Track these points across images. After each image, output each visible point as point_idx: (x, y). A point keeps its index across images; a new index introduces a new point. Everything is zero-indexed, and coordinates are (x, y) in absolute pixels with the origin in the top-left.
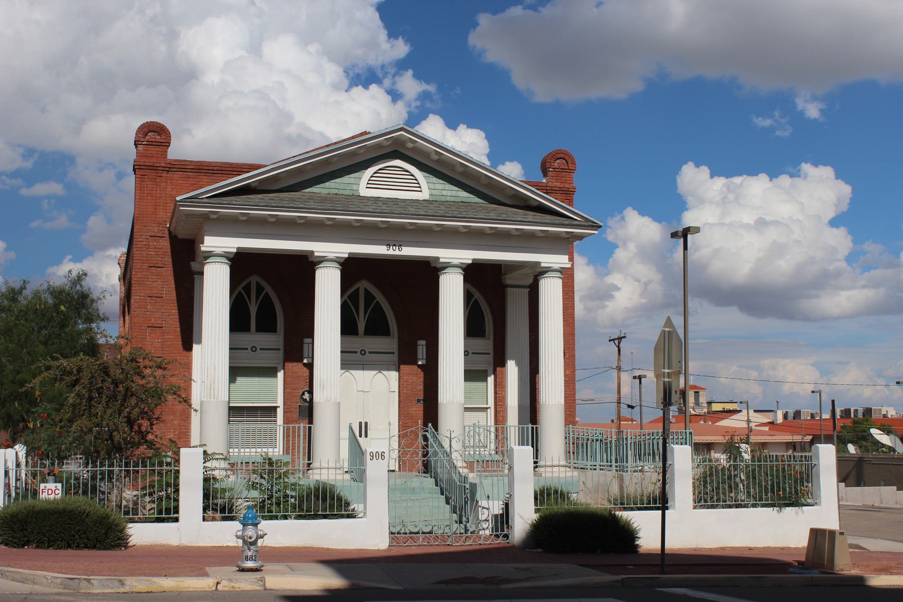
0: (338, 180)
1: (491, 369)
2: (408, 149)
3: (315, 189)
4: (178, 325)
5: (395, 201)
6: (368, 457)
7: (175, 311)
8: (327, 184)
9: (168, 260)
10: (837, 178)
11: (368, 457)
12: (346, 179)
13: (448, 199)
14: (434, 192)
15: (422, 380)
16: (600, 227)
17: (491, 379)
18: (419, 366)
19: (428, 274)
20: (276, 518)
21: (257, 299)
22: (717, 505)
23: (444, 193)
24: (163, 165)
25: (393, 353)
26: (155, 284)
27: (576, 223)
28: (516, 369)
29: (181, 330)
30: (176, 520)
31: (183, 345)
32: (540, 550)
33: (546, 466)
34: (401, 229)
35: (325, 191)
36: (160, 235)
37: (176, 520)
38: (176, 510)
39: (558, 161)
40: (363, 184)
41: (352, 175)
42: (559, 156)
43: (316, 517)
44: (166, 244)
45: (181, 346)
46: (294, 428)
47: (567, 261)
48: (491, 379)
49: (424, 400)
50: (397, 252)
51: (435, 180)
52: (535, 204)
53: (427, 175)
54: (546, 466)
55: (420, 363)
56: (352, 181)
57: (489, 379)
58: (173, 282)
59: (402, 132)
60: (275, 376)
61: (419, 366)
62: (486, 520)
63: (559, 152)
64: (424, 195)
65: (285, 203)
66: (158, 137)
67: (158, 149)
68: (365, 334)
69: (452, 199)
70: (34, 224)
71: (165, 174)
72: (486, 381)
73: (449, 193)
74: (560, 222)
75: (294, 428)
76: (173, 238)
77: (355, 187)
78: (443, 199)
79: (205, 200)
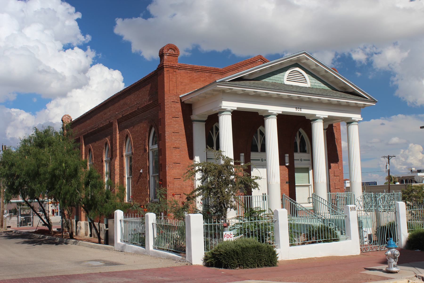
0: (275, 76)
2: (301, 63)
6: (350, 210)
7: (185, 140)
8: (271, 78)
9: (180, 114)
10: (109, 69)
12: (278, 76)
13: (318, 87)
14: (313, 84)
15: (287, 173)
18: (286, 166)
22: (107, 232)
23: (316, 84)
24: (177, 66)
25: (309, 160)
26: (176, 126)
29: (188, 150)
30: (291, 245)
32: (418, 250)
35: (271, 81)
36: (176, 101)
40: (285, 78)
41: (281, 74)
44: (179, 106)
46: (247, 197)
47: (360, 117)
48: (311, 172)
49: (289, 182)
50: (300, 112)
51: (312, 78)
52: (351, 91)
55: (287, 165)
56: (281, 77)
57: (310, 171)
58: (183, 125)
60: (308, 172)
61: (286, 166)
62: (366, 237)
64: (308, 85)
66: (174, 52)
67: (173, 58)
71: (177, 71)
73: (317, 84)
76: (183, 104)
77: (282, 80)
78: (315, 87)
79: (229, 83)
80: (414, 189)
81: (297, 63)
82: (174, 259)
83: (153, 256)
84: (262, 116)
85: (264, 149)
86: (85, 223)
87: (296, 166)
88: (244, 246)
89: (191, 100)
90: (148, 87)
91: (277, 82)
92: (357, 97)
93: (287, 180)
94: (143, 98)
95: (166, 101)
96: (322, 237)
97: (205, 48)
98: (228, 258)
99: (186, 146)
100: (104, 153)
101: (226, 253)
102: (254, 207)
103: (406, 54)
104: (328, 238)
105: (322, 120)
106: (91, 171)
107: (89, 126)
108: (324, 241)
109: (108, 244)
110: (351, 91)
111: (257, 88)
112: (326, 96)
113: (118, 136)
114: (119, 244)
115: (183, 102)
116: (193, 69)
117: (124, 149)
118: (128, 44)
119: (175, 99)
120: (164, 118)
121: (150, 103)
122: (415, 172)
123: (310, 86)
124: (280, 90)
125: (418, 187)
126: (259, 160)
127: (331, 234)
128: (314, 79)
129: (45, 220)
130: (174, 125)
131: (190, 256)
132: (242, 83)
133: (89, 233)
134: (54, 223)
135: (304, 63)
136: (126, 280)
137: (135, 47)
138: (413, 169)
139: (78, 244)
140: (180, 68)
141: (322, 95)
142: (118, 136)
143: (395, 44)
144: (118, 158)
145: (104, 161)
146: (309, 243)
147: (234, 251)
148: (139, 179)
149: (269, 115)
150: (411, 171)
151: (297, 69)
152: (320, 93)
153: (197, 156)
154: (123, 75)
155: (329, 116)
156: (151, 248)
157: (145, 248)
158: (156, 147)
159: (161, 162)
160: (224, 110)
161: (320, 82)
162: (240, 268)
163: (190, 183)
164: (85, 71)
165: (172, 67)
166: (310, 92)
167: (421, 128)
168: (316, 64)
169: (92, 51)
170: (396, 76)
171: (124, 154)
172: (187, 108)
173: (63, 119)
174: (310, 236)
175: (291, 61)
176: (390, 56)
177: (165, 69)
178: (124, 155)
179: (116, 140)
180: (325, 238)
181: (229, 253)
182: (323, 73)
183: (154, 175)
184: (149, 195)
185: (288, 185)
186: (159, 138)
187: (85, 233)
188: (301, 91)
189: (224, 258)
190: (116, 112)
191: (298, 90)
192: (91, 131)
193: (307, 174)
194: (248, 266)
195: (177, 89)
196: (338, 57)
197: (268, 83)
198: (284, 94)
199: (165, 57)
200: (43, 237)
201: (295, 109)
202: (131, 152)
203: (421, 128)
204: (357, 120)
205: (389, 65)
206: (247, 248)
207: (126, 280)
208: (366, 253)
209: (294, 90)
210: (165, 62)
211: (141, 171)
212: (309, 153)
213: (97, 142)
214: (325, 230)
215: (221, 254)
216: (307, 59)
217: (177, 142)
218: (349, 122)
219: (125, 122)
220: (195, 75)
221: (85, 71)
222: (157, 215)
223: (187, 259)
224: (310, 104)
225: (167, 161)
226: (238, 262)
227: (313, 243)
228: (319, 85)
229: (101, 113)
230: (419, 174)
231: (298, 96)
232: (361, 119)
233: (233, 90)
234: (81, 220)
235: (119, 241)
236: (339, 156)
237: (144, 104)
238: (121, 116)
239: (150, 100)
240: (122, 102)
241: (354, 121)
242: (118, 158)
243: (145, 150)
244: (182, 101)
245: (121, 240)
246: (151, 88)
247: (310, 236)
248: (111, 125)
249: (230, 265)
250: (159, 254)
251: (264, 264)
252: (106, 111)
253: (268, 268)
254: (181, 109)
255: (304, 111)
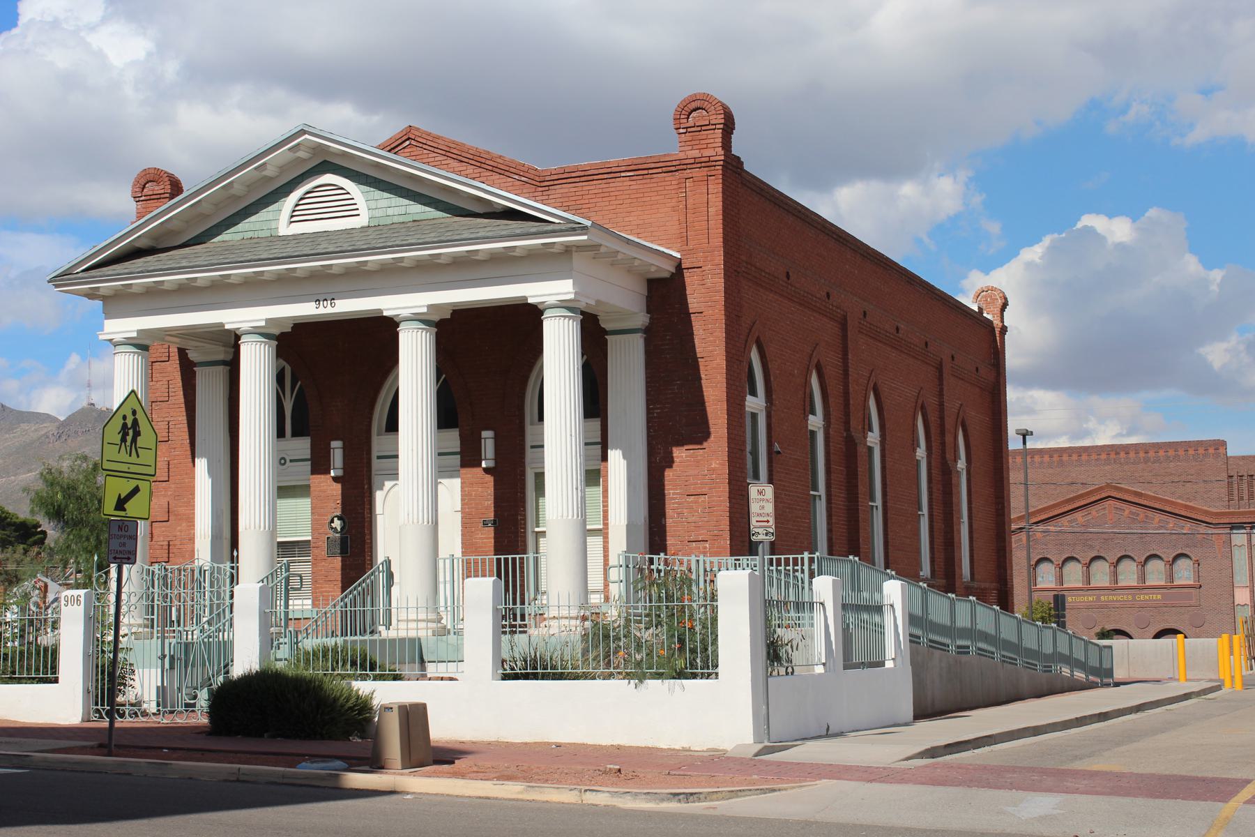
0: (253, 218)
3: (226, 236)
8: (240, 227)
13: (396, 220)
15: (491, 491)
19: (379, 336)
23: (390, 211)
27: (550, 227)
28: (208, 482)
30: (56, 681)
33: (428, 621)
35: (239, 237)
37: (56, 681)
38: (54, 669)
39: (694, 114)
40: (281, 220)
41: (270, 208)
42: (694, 105)
43: (19, 681)
46: (506, 560)
50: (329, 310)
51: (378, 194)
54: (428, 621)
59: (307, 136)
63: (694, 99)
65: (200, 261)
69: (401, 219)
70: (1088, 220)
73: (397, 211)
74: (534, 230)
75: (506, 560)
81: (325, 161)
93: (491, 516)
102: (153, 671)
128: (386, 195)
132: (139, 263)
134: (264, 654)
151: (328, 178)
161: (406, 202)
185: (490, 532)
197: (229, 247)
224: (359, 280)
228: (402, 210)
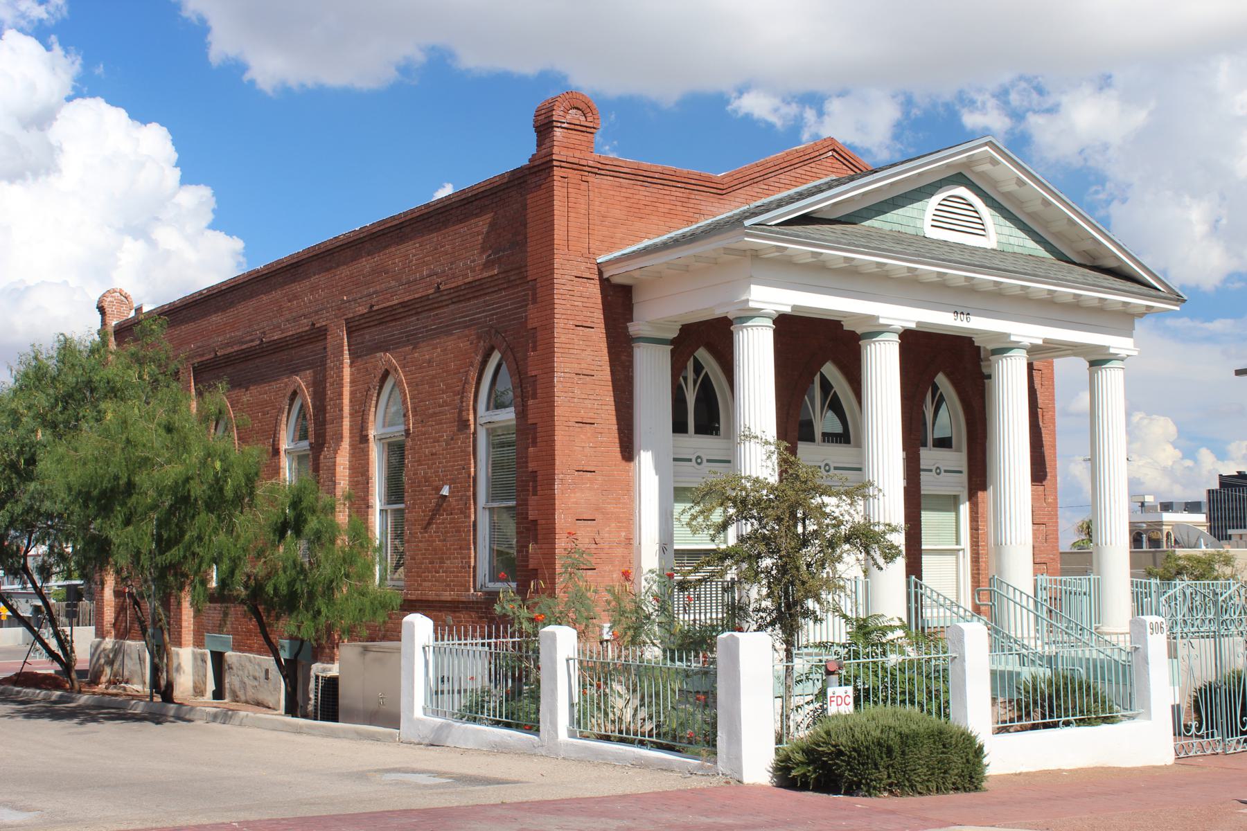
0: (900, 211)
1: (964, 494)
4: (615, 421)
5: (962, 247)
6: (1149, 630)
7: (610, 399)
8: (889, 216)
9: (599, 315)
11: (1149, 630)
13: (1017, 250)
16: (1184, 301)
17: (965, 509)
20: (1055, 725)
21: (695, 382)
23: (1012, 240)
24: (591, 163)
25: (960, 472)
31: (622, 452)
34: (970, 289)
35: (887, 227)
40: (924, 218)
41: (915, 205)
44: (594, 290)
45: (619, 455)
47: (1131, 346)
50: (965, 324)
51: (1001, 220)
53: (994, 213)
58: (605, 351)
59: (987, 148)
60: (956, 510)
64: (989, 242)
66: (583, 118)
68: (696, 432)
71: (591, 178)
72: (957, 511)
76: (605, 284)
79: (777, 229)
80: (1184, 567)
82: (666, 768)
83: (564, 757)
84: (853, 332)
85: (845, 436)
86: (194, 654)
87: (925, 490)
88: (907, 731)
89: (637, 274)
90: (482, 224)
91: (903, 229)
92: (1129, 284)
94: (464, 255)
95: (557, 274)
96: (1066, 710)
97: (472, 60)
98: (863, 764)
99: (614, 418)
100: (283, 426)
101: (854, 750)
103: (1140, 117)
104: (1089, 711)
105: (1024, 353)
106: (300, 489)
107: (222, 333)
108: (1081, 722)
109: (336, 720)
110: (1111, 264)
111: (853, 246)
112: (1045, 278)
113: (347, 372)
114: (419, 720)
115: (607, 279)
116: (640, 176)
117: (371, 418)
118: (200, 31)
119: (583, 268)
120: (549, 327)
121: (485, 275)
122: (1153, 508)
123: (994, 246)
124: (919, 256)
125: (1199, 560)
126: (690, 460)
127: (1088, 695)
128: (1008, 223)
129: (53, 644)
130: (579, 350)
131: (736, 759)
133: (211, 686)
135: (983, 175)
136: (615, 823)
137: (223, 43)
138: (1149, 499)
139: (236, 721)
140: (600, 169)
141: (1033, 276)
142: (347, 372)
143: (1104, 83)
144: (346, 444)
145: (282, 453)
146: (1024, 729)
147: (879, 744)
148: (431, 519)
149: (875, 333)
150: (1143, 504)
151: (962, 191)
152: (1029, 270)
153: (647, 449)
154: (175, 142)
155: (1046, 341)
156: (563, 734)
157: (538, 735)
158: (507, 416)
159: (532, 466)
160: (755, 314)
161: (1023, 235)
162: (891, 792)
163: (623, 534)
164: (41, 120)
165: (577, 167)
166: (1002, 265)
167: (1238, 373)
168: (1019, 179)
169: (67, 52)
170: (1108, 185)
171: (372, 433)
172: (618, 300)
173: (106, 305)
174: (1027, 706)
175: (948, 165)
176: (1086, 121)
177: (557, 172)
178: (371, 437)
179: (341, 386)
180: (1081, 712)
181: (867, 748)
182: (1037, 207)
183: (495, 505)
184: (475, 567)
186: (531, 390)
187: (195, 688)
188: (976, 260)
189: (848, 763)
190: (342, 293)
191: (966, 257)
192: (229, 350)
193: (953, 514)
194: (912, 786)
195: (591, 236)
196: (916, 112)
197: (882, 235)
198: (928, 269)
199: (558, 133)
200: (61, 700)
201: (951, 315)
202: (402, 428)
203: (1238, 373)
204: (1123, 353)
205: (1081, 152)
206: (916, 735)
207: (626, 823)
208: (1189, 761)
209: (956, 257)
210: (556, 150)
211: (445, 491)
212: (959, 450)
213: (254, 390)
214: (1081, 689)
215: (840, 753)
216: (994, 162)
217: (588, 403)
218: (1098, 360)
219: (377, 329)
220: (643, 193)
221: (41, 120)
222: (581, 635)
223: (721, 767)
225: (557, 462)
226: (889, 777)
227: (1034, 727)
228: (1021, 242)
229: (277, 294)
230: (1167, 517)
231: (966, 277)
232: (1135, 353)
233: (786, 252)
234: (180, 645)
235: (418, 713)
236: (1047, 459)
237: (466, 276)
238: (363, 310)
239: (488, 265)
240: (366, 264)
241: (1115, 357)
242: (346, 444)
243: (464, 424)
244: (606, 275)
245: (424, 709)
246: (492, 225)
247: (1027, 706)
248: (318, 334)
249: (868, 784)
250: (597, 753)
251: (954, 784)
252: (296, 287)
253: (961, 797)
254: (600, 301)
255: (978, 324)
